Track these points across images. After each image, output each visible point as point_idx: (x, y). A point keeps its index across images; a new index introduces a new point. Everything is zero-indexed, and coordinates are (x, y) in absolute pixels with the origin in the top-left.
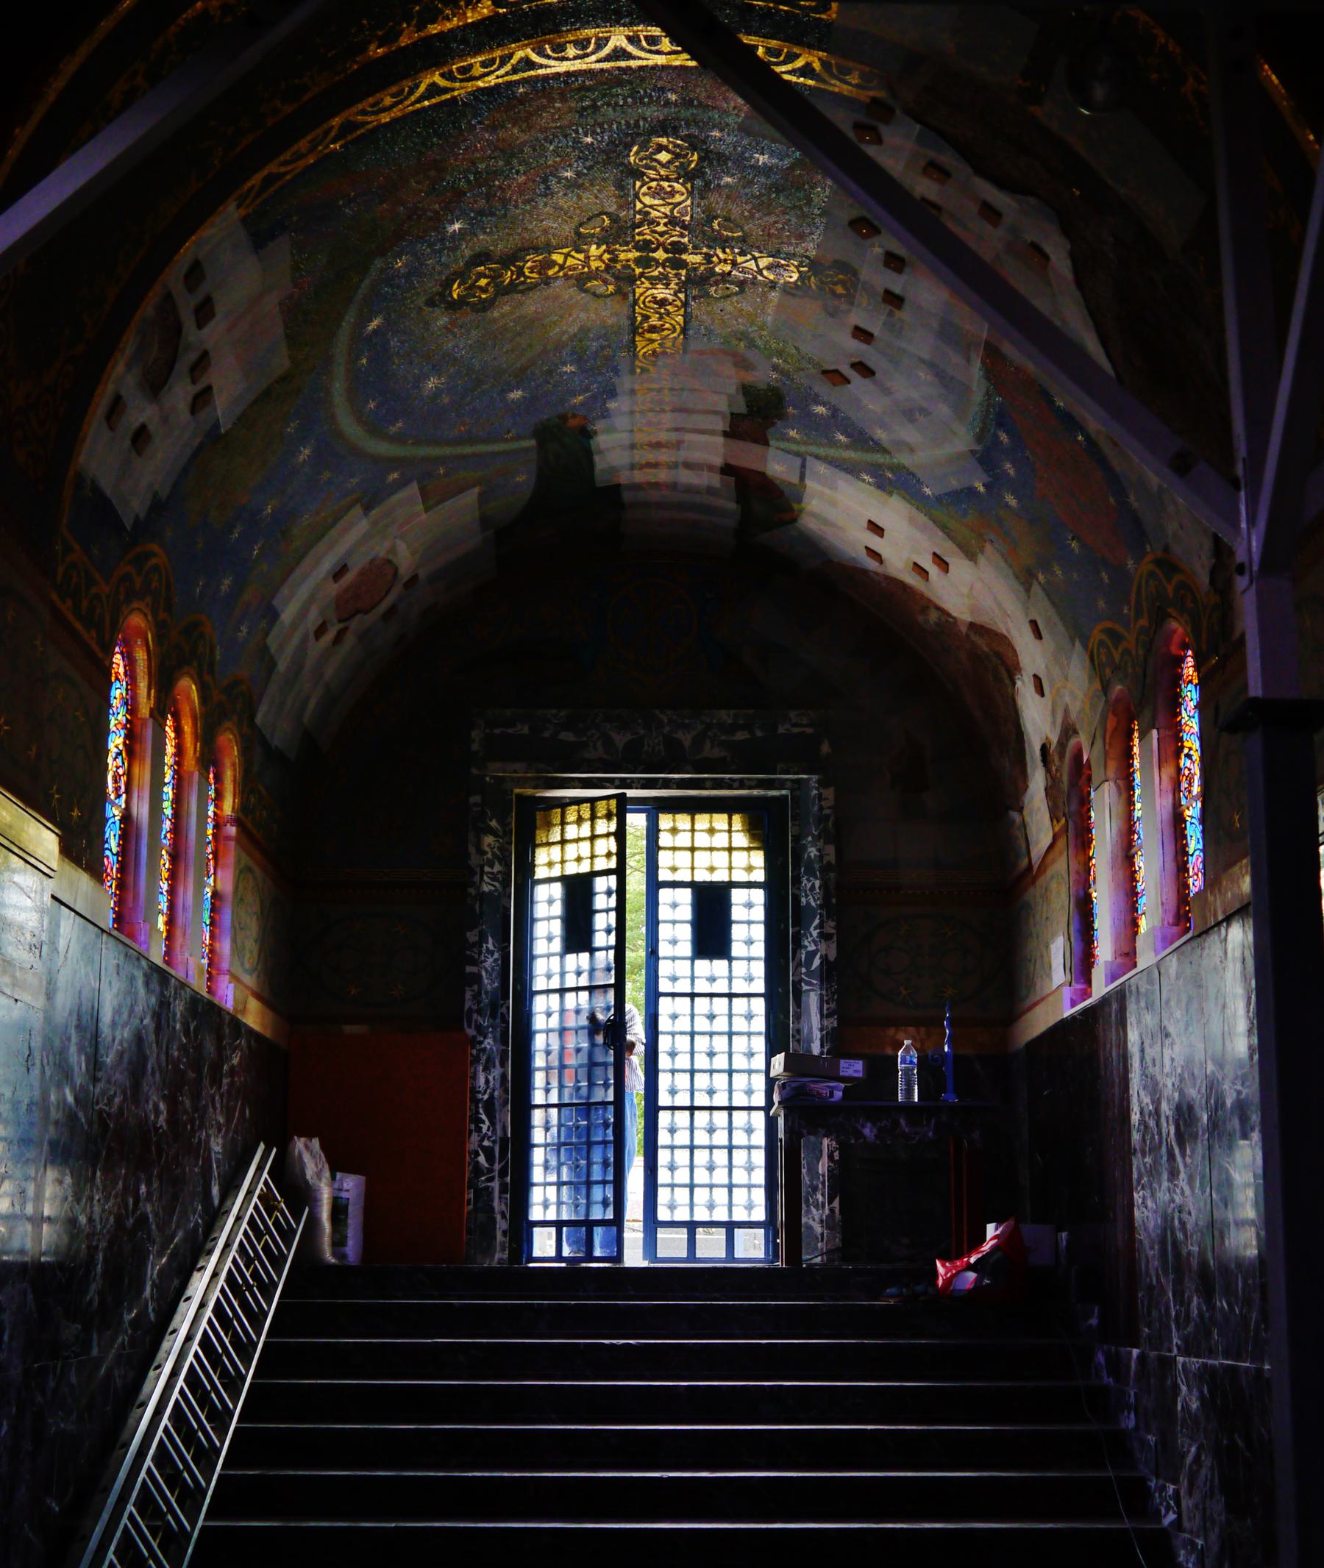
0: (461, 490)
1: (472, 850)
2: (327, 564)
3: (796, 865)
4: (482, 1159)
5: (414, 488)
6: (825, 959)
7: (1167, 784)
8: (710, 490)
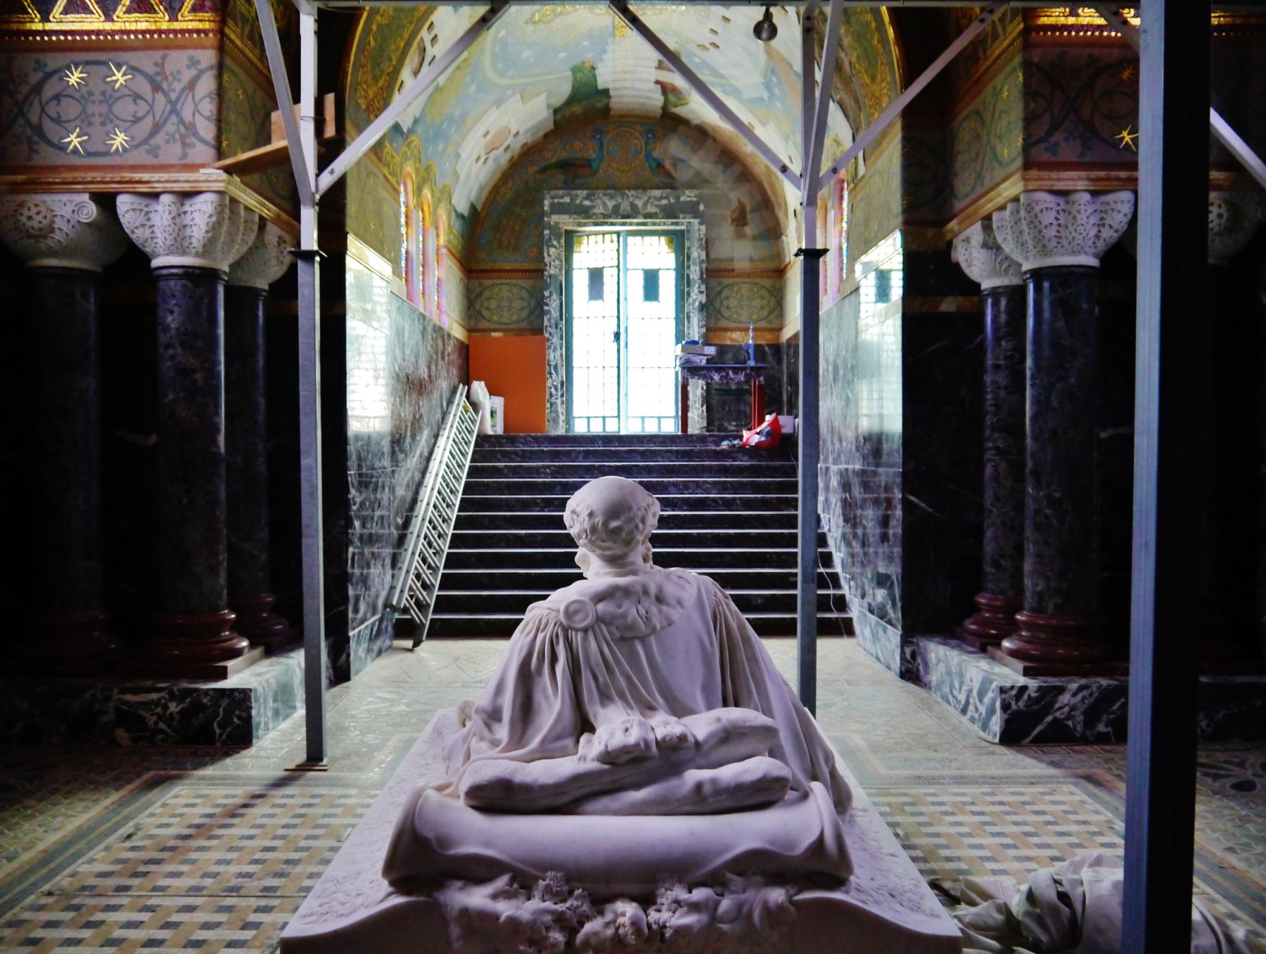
0: (538, 95)
2: (482, 131)
5: (518, 96)
6: (701, 303)
7: (837, 234)
8: (650, 90)
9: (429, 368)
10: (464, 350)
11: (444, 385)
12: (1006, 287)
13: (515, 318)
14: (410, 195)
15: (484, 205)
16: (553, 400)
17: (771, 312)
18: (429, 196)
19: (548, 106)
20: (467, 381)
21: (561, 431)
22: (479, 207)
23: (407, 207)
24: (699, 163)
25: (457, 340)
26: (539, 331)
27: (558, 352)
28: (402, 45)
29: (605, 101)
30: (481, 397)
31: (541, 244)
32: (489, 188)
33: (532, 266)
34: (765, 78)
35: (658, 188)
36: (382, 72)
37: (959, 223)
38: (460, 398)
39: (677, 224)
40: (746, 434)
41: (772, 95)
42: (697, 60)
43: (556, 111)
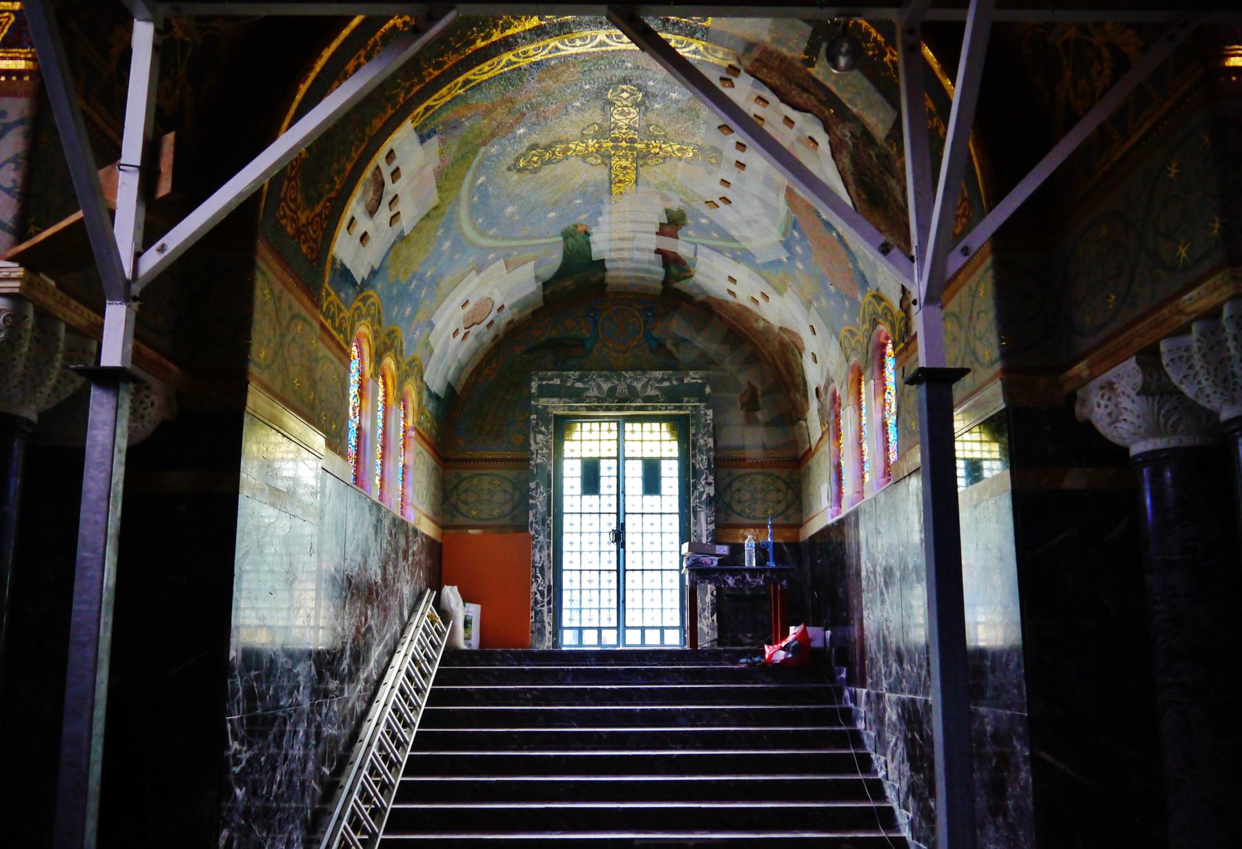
0: (525, 262)
1: (532, 442)
2: (460, 300)
3: (694, 448)
4: (538, 596)
5: (501, 263)
7: (879, 407)
8: (650, 262)
9: (384, 569)
10: (435, 550)
11: (407, 590)
12: (1174, 449)
13: (496, 512)
14: (367, 361)
15: (464, 388)
16: (538, 608)
17: (788, 506)
18: (393, 367)
19: (537, 278)
20: (436, 583)
21: (547, 645)
22: (458, 389)
23: (362, 375)
24: (705, 343)
25: (427, 537)
26: (523, 527)
27: (545, 553)
28: (349, 167)
29: (600, 275)
30: (453, 605)
31: (526, 430)
32: (470, 369)
33: (518, 455)
34: (784, 235)
35: (659, 369)
36: (321, 195)
37: (1090, 367)
38: (426, 607)
39: (680, 408)
40: (768, 650)
41: (792, 255)
42: (704, 221)
43: (546, 285)
